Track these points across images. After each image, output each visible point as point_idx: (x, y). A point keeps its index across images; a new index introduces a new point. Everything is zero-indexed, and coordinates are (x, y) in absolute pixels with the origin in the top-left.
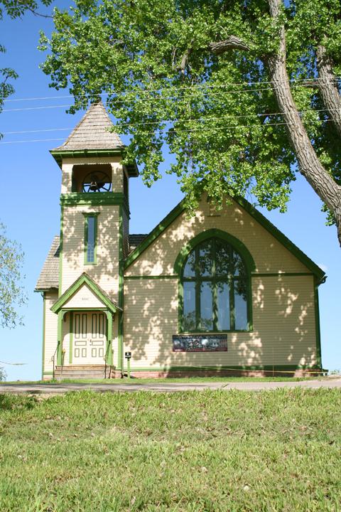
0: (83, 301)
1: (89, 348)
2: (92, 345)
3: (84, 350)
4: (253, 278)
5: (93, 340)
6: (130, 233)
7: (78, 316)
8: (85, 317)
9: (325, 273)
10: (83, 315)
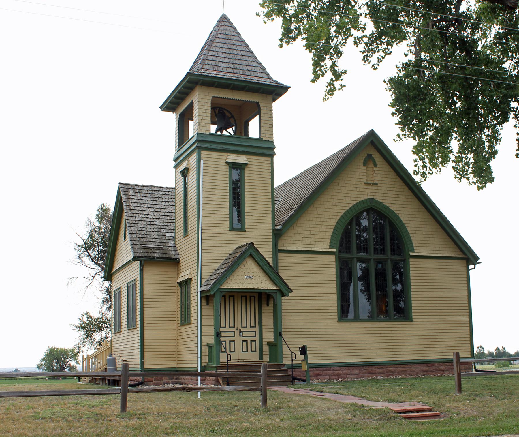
0: (247, 281)
3: (232, 343)
4: (411, 260)
5: (243, 329)
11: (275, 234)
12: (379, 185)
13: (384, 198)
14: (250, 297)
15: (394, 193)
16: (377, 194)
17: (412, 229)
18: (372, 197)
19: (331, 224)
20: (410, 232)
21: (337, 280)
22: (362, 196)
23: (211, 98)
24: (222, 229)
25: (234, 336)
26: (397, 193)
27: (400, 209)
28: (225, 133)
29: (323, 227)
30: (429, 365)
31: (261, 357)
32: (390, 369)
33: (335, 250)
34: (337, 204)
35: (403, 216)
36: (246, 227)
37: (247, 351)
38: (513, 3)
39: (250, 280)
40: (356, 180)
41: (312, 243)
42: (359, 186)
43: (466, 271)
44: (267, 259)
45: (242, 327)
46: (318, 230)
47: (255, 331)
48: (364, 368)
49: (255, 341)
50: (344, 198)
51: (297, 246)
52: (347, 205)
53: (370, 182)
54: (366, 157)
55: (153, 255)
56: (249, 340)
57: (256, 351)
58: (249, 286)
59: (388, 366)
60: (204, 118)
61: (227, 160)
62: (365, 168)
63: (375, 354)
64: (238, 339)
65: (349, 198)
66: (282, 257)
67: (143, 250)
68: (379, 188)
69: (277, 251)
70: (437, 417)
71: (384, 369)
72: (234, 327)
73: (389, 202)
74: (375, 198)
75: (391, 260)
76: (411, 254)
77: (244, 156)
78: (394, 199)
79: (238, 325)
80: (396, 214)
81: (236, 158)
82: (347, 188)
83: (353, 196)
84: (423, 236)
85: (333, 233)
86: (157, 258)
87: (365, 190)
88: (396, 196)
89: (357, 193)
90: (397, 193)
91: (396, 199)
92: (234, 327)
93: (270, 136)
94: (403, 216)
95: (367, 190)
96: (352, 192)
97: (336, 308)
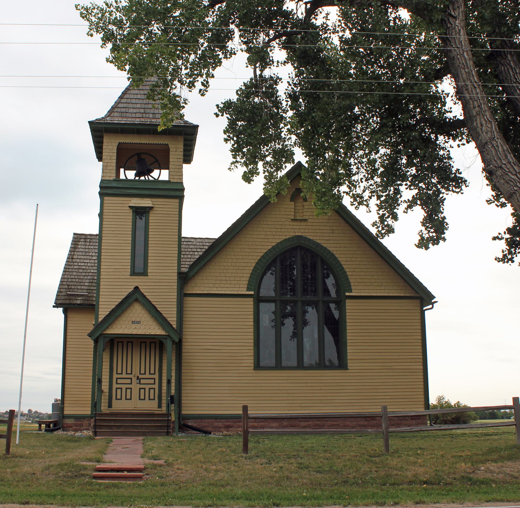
0: (134, 326)
1: (135, 387)
2: (140, 383)
3: (129, 391)
4: (347, 301)
5: (141, 376)
6: (512, 404)
7: (120, 344)
8: (130, 344)
9: (435, 297)
10: (118, 342)
11: (180, 277)
12: (309, 220)
13: (315, 234)
14: (151, 343)
15: (328, 228)
16: (306, 231)
17: (350, 266)
18: (300, 234)
19: (249, 264)
20: (346, 270)
21: (254, 325)
22: (288, 234)
23: (117, 144)
24: (122, 274)
25: (131, 384)
26: (331, 228)
27: (335, 245)
28: (142, 178)
29: (240, 268)
30: (368, 419)
31: (160, 406)
32: (318, 422)
33: (252, 293)
34: (258, 243)
35: (339, 252)
36: (149, 271)
37: (144, 399)
38: (358, 3)
39: (138, 326)
40: (282, 216)
41: (226, 286)
42: (285, 223)
43: (419, 311)
44: (153, 303)
45: (140, 374)
46: (234, 271)
47: (154, 379)
48: (285, 420)
49: (154, 389)
50: (266, 237)
51: (208, 289)
52: (270, 244)
53: (298, 218)
54: (294, 192)
55: (75, 302)
56: (147, 387)
57: (154, 399)
58: (135, 332)
59: (316, 419)
60: (109, 164)
61: (130, 205)
62: (293, 203)
63: (299, 405)
64: (135, 387)
65: (272, 237)
66: (190, 302)
67: (67, 297)
68: (309, 224)
69: (182, 295)
70: (138, 479)
71: (310, 423)
72: (131, 374)
73: (321, 238)
74: (304, 234)
75: (323, 301)
76: (347, 294)
77: (149, 199)
78: (327, 235)
79: (136, 372)
80: (330, 251)
81: (140, 202)
82: (270, 226)
83: (277, 233)
84: (364, 274)
85: (251, 274)
86: (78, 304)
87: (291, 227)
88: (331, 231)
89: (282, 230)
90: (331, 228)
91: (331, 235)
92: (131, 374)
93: (179, 177)
94: (339, 252)
95: (295, 227)
96: (276, 230)
97: (253, 354)
